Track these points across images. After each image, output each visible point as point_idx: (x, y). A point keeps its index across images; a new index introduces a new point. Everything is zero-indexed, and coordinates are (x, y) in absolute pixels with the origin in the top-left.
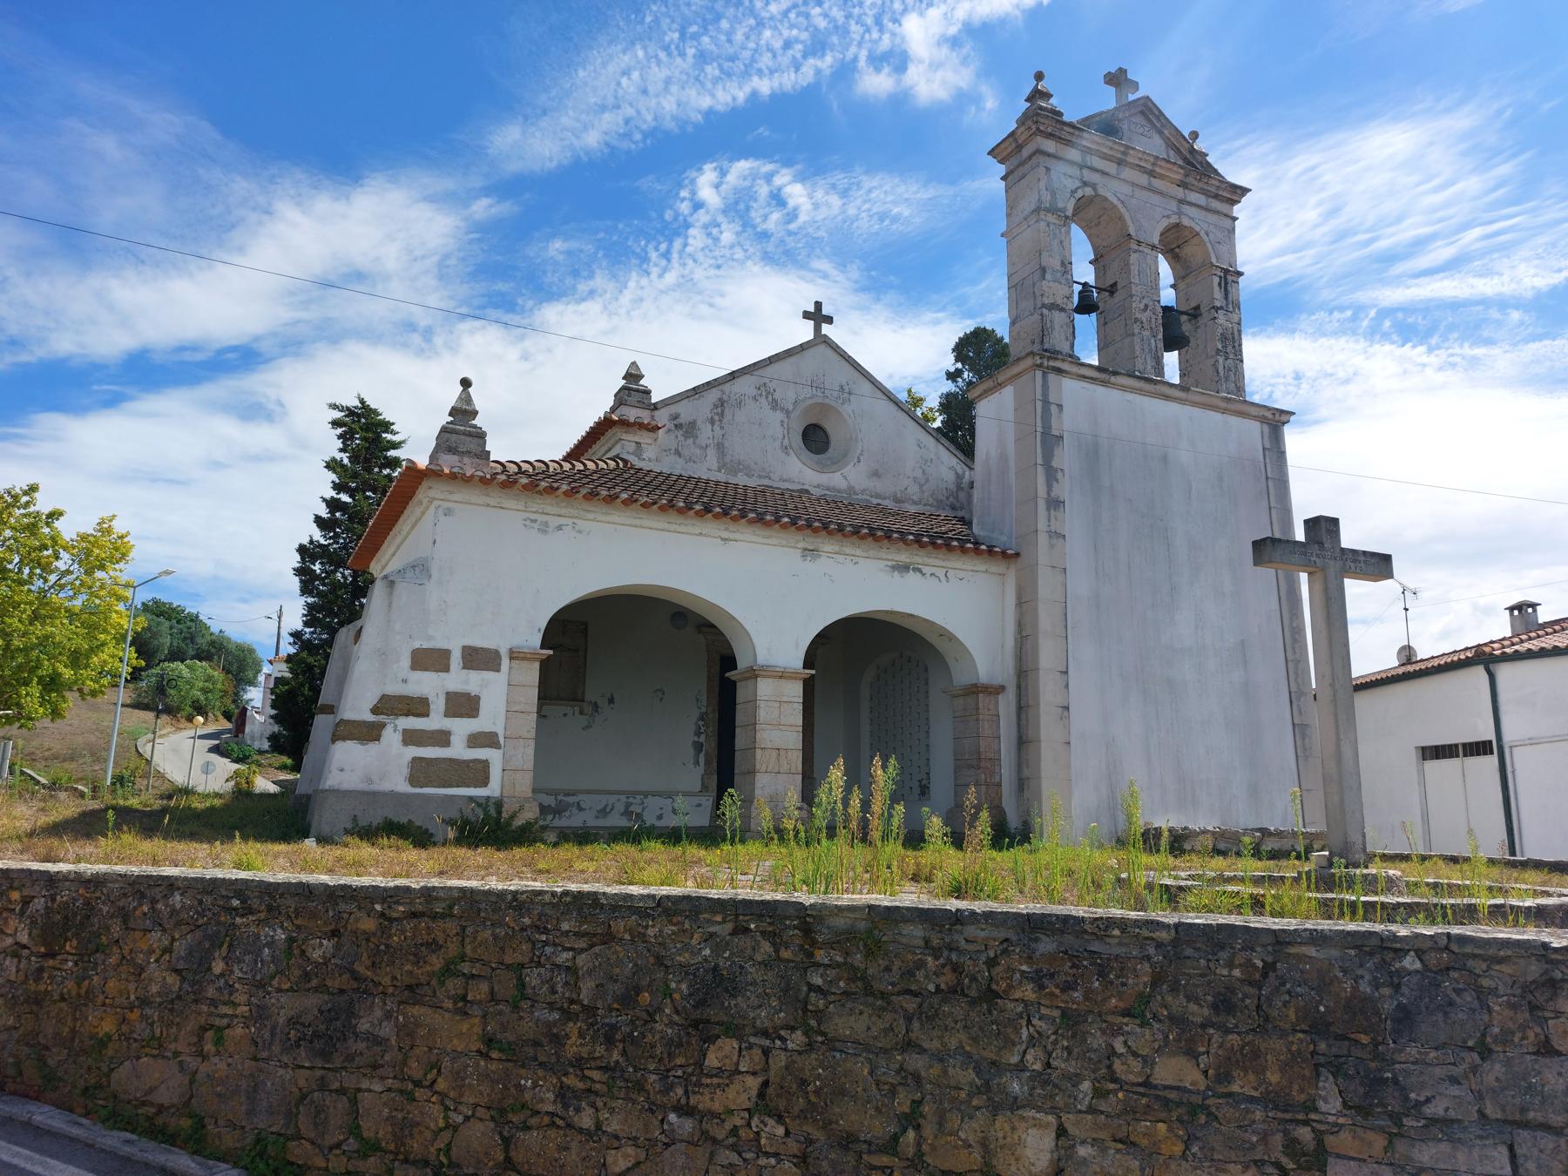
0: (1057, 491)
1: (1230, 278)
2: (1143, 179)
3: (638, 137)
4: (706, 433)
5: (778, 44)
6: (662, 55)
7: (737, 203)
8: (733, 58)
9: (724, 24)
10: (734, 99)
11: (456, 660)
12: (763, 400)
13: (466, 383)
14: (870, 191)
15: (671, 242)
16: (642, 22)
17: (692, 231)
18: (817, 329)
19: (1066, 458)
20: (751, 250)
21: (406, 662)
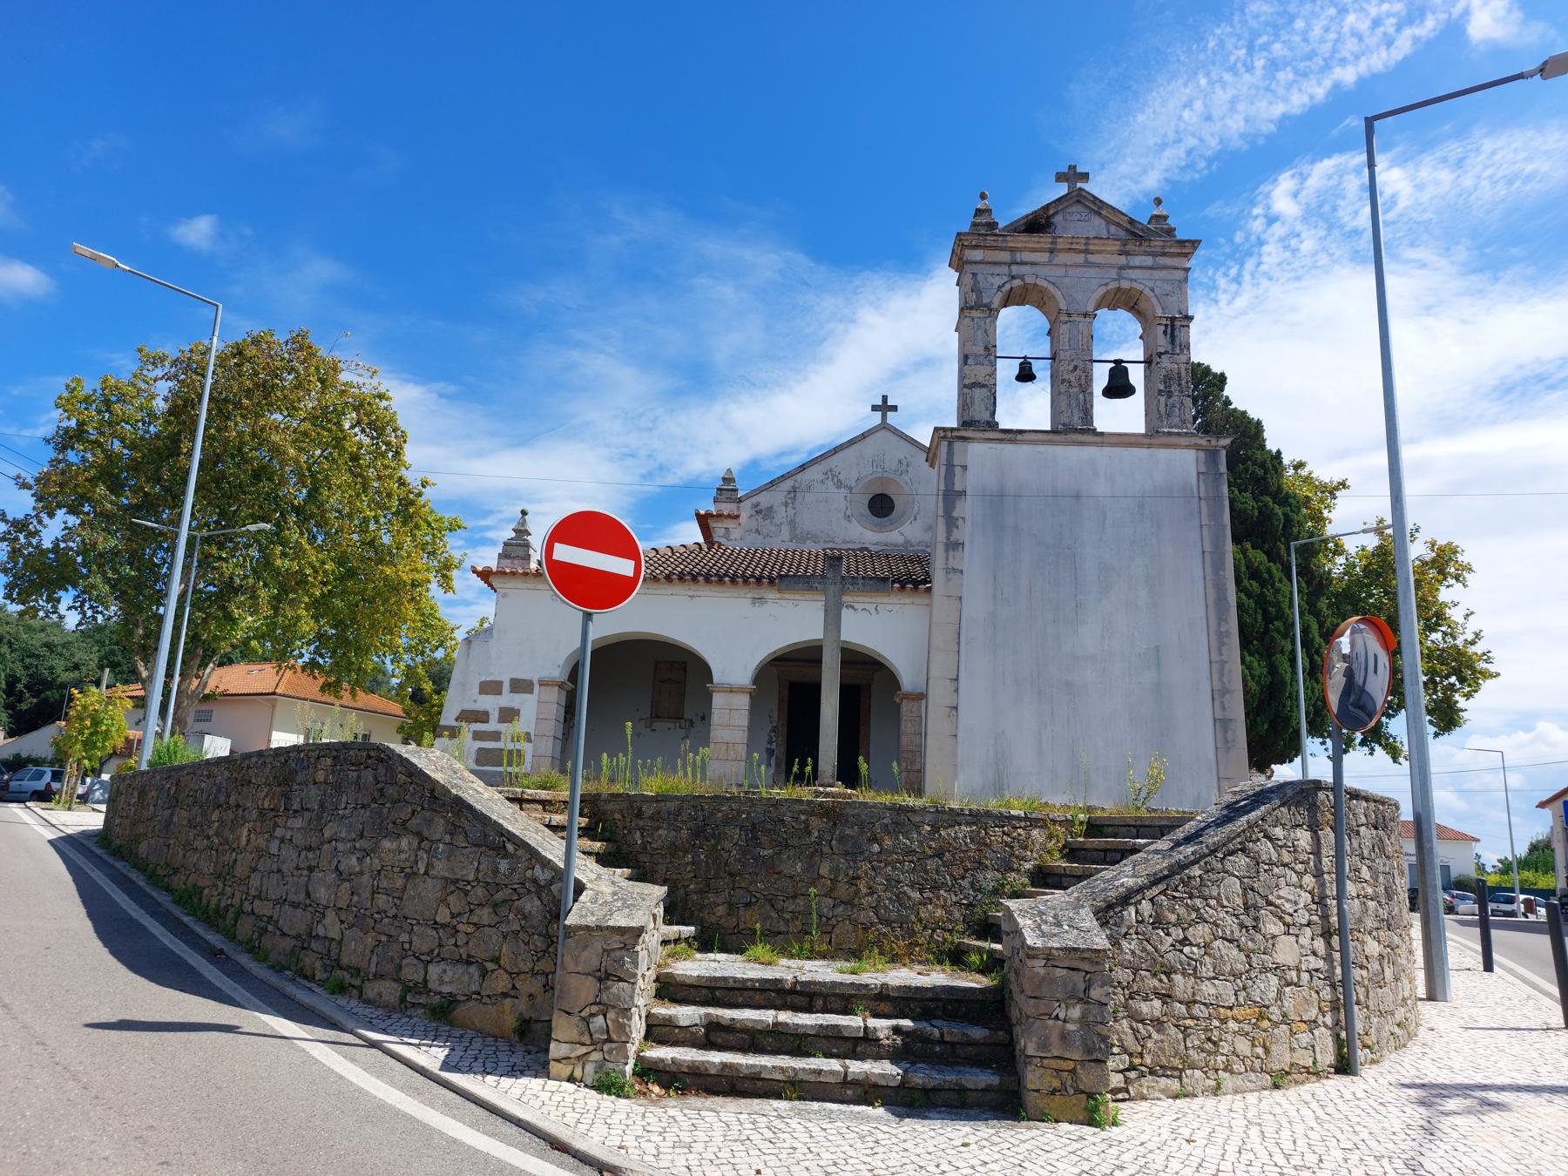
0: (956, 535)
1: (1177, 324)
2: (1080, 258)
3: (1202, 164)
4: (781, 514)
5: (1363, 26)
6: (1227, 77)
7: (1320, 206)
8: (1308, 57)
9: (1299, 24)
10: (1312, 97)
11: (506, 687)
12: (829, 483)
13: (524, 513)
14: (1494, 153)
15: (1242, 265)
16: (1205, 50)
17: (1265, 249)
18: (884, 417)
19: (967, 509)
20: (1339, 253)
21: (476, 689)
